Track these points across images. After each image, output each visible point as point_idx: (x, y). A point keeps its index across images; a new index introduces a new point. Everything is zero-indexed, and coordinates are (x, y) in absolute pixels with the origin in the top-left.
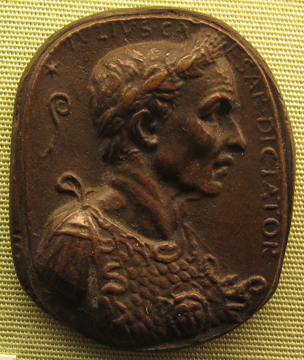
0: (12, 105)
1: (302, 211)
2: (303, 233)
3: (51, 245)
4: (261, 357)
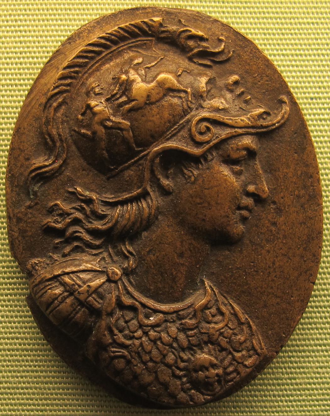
0: (5, 157)
1: (328, 301)
2: (329, 175)
3: (91, 27)
4: (303, 413)
